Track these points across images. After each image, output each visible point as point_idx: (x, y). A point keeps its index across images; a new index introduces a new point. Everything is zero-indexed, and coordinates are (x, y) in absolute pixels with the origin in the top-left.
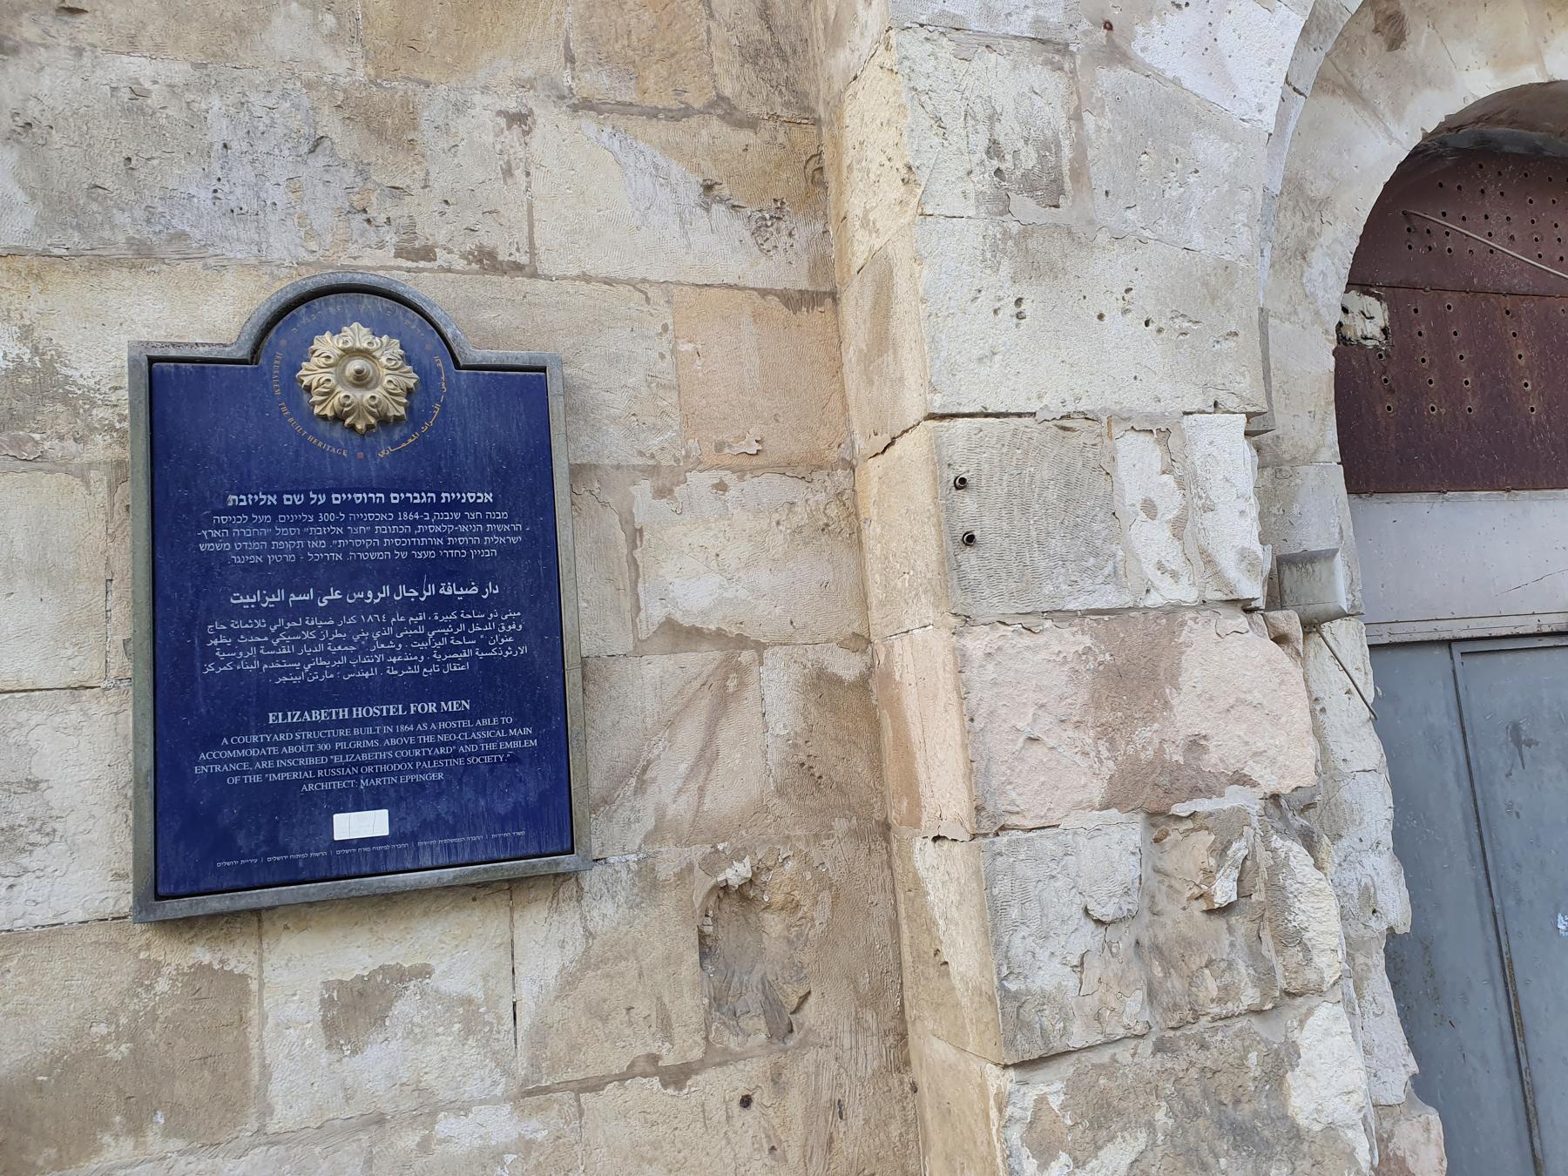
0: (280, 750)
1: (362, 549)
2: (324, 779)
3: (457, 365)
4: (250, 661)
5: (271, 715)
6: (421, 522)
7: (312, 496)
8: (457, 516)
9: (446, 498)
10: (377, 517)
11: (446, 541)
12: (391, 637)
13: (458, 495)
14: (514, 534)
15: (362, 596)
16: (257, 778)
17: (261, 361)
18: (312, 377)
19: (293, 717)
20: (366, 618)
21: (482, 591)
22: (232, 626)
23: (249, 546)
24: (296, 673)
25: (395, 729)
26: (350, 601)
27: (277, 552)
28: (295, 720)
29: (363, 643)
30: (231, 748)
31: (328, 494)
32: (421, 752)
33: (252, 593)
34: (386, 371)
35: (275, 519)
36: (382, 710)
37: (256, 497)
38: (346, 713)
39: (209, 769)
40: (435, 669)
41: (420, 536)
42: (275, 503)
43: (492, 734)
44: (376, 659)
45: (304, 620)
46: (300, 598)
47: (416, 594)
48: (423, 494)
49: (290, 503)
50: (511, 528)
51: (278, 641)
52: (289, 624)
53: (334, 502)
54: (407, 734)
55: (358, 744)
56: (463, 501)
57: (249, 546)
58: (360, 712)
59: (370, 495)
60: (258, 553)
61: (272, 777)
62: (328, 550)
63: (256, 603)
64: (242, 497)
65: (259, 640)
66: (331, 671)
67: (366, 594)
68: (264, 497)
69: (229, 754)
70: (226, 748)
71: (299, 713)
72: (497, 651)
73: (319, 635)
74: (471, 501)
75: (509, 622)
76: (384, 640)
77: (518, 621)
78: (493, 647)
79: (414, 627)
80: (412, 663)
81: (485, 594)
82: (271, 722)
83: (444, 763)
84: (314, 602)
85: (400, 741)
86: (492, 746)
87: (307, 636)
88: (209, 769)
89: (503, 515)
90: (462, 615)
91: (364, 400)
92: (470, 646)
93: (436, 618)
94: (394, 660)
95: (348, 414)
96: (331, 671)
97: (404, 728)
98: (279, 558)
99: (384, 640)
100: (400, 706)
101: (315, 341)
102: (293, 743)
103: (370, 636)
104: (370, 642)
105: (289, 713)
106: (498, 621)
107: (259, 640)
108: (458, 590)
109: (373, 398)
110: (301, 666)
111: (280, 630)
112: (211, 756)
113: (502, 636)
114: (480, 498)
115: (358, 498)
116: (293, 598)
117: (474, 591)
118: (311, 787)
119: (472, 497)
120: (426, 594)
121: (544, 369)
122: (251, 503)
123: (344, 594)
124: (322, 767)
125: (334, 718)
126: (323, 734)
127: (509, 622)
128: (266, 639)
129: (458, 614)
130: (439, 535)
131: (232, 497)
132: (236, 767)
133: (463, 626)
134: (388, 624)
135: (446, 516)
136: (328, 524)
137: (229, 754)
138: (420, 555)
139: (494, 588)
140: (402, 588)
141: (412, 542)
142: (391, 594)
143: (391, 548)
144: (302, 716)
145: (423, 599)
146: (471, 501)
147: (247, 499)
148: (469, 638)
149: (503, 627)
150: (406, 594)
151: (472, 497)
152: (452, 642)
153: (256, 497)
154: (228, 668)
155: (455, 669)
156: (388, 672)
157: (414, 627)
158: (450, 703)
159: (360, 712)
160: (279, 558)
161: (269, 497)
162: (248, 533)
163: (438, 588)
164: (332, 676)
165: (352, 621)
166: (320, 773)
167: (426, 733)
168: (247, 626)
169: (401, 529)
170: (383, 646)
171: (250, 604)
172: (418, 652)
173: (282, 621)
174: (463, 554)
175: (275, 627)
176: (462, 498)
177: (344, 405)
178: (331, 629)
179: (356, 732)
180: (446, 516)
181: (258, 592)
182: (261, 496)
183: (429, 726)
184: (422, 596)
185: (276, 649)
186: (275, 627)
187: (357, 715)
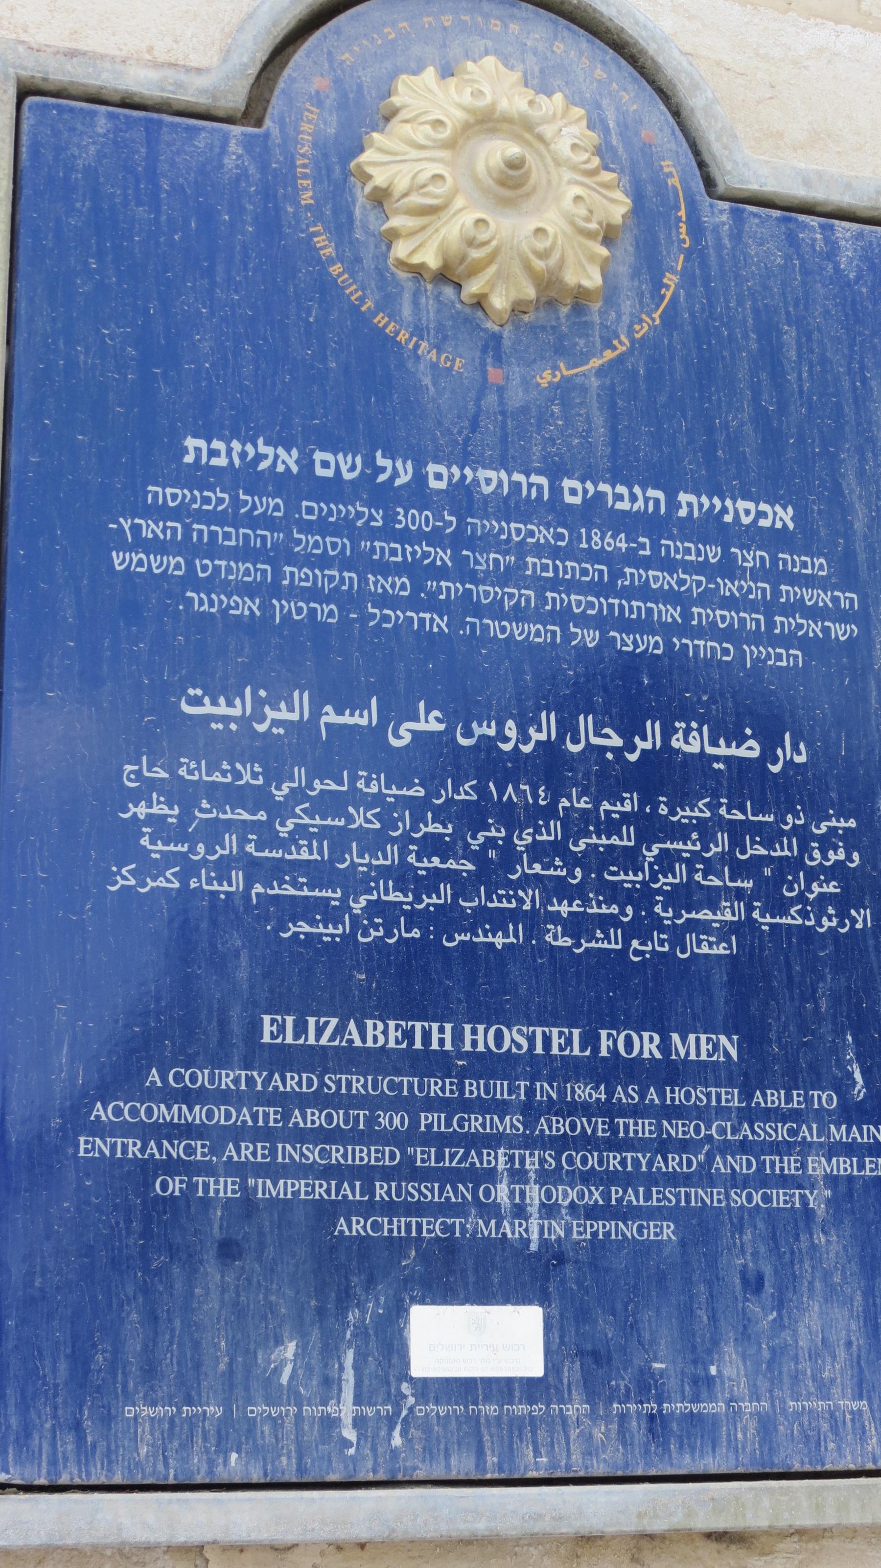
0: (286, 1116)
1: (496, 611)
2: (390, 1209)
3: (709, 183)
4: (223, 869)
5: (267, 1019)
6: (632, 558)
7: (381, 461)
8: (713, 554)
9: (690, 505)
10: (531, 534)
11: (687, 615)
12: (559, 848)
13: (716, 501)
14: (843, 617)
15: (492, 732)
17: (268, 123)
18: (394, 168)
19: (320, 1031)
20: (501, 791)
21: (768, 755)
22: (182, 772)
23: (229, 570)
24: (332, 916)
25: (562, 1092)
26: (464, 742)
27: (293, 593)
28: (324, 1041)
29: (492, 854)
30: (169, 1096)
31: (556, 473)
32: (623, 1162)
33: (232, 693)
34: (567, 175)
35: (292, 506)
36: (531, 1039)
37: (249, 448)
38: (448, 1036)
39: (113, 1147)
40: (658, 944)
41: (628, 593)
42: (295, 469)
43: (791, 1132)
44: (521, 901)
45: (354, 779)
46: (346, 719)
47: (617, 741)
48: (637, 490)
49: (329, 473)
50: (835, 600)
51: (290, 824)
52: (317, 784)
53: (433, 484)
54: (587, 1109)
55: (475, 1124)
57: (229, 570)
58: (480, 1037)
60: (249, 590)
62: (413, 602)
63: (241, 720)
64: (217, 444)
65: (246, 816)
66: (412, 920)
67: (501, 726)
68: (269, 450)
69: (162, 1113)
70: (151, 1095)
71: (334, 1022)
72: (804, 914)
73: (389, 823)
74: (746, 520)
75: (827, 843)
76: (537, 852)
77: (850, 840)
78: (792, 901)
79: (611, 827)
80: (606, 922)
81: (775, 762)
82: (266, 1039)
85: (573, 1127)
87: (359, 821)
88: (113, 1147)
89: (819, 567)
90: (723, 811)
92: (739, 894)
93: (663, 810)
94: (564, 909)
95: (475, 270)
96: (412, 920)
97: (583, 1092)
98: (299, 611)
99: (537, 852)
100: (576, 1032)
101: (400, 87)
102: (320, 1100)
103: (508, 839)
104: (509, 856)
105: (312, 1021)
106: (803, 835)
107: (246, 816)
108: (714, 743)
109: (540, 232)
110: (344, 900)
111: (298, 795)
112: (118, 1112)
113: (812, 875)
114: (764, 515)
115: (488, 481)
116: (330, 716)
117: (750, 750)
118: (358, 1226)
119: (747, 512)
120: (641, 745)
122: (237, 462)
123: (449, 718)
124: (387, 1174)
125: (418, 1045)
126: (392, 1086)
127: (827, 843)
128: (262, 816)
129: (713, 807)
130: (670, 597)
131: (191, 443)
132: (177, 1150)
133: (723, 839)
134: (550, 812)
135: (688, 551)
136: (419, 537)
137: (162, 1113)
138: (626, 643)
139: (796, 749)
140: (585, 723)
141: (611, 606)
142: (561, 737)
143: (563, 617)
144: (340, 1030)
145: (633, 757)
146: (746, 520)
147: (229, 451)
148: (739, 870)
149: (817, 854)
150: (595, 741)
151: (747, 512)
152: (698, 877)
153: (249, 448)
154: (169, 881)
155: (705, 950)
156: (549, 938)
157: (611, 827)
158: (692, 1037)
159: (480, 1037)
160: (299, 611)
161: (281, 451)
162: (227, 536)
163: (668, 732)
164: (416, 933)
165: (467, 793)
166: (380, 1191)
167: (636, 1112)
168: (217, 777)
169: (585, 572)
170: (537, 868)
172: (613, 894)
173: (300, 773)
174: (726, 652)
175: (286, 788)
176: (724, 510)
177: (471, 243)
178: (419, 809)
179: (473, 1089)
180: (688, 551)
181: (248, 691)
182: (263, 449)
183: (643, 1095)
184: (632, 748)
185: (284, 844)
186: (286, 788)
187: (474, 1043)
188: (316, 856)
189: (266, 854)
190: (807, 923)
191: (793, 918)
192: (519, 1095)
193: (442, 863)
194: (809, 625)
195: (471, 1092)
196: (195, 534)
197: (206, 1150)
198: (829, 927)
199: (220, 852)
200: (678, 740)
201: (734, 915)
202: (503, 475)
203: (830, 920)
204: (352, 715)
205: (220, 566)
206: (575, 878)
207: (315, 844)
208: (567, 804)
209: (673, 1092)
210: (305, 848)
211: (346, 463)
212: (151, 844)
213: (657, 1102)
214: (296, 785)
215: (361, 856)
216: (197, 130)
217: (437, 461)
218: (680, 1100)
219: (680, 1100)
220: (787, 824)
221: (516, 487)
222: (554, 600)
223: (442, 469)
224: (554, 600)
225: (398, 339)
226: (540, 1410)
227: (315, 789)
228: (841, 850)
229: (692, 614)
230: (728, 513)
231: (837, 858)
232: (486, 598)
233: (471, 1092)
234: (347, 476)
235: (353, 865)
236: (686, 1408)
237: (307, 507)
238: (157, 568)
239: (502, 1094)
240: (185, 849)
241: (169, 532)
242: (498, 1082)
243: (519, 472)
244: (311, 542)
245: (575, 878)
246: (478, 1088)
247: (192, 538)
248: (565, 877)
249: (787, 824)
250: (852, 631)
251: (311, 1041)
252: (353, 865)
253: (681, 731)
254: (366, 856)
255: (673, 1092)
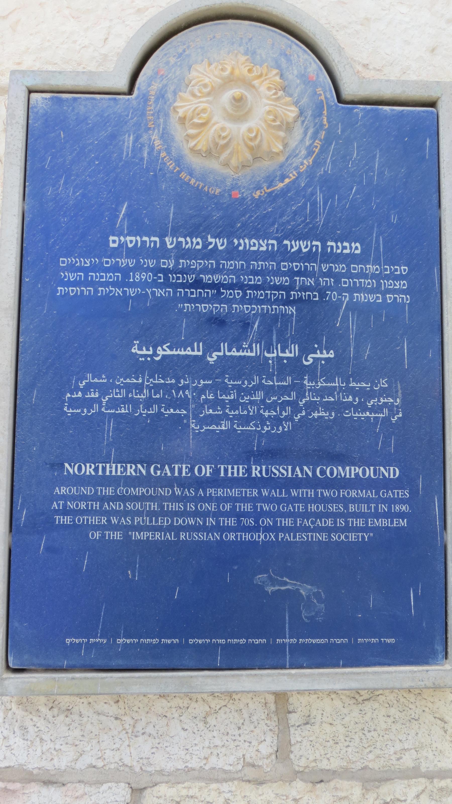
3: (340, 99)
16: (117, 536)
56: (241, 248)
59: (145, 238)
61: (136, 536)
64: (346, 244)
83: (308, 536)
84: (297, 360)
86: (360, 523)
91: (241, 132)
109: (250, 130)
121: (433, 104)
160: (205, 308)
171: (146, 356)
188: (127, 411)
189: (109, 411)
190: (258, 429)
191: (252, 427)
192: (371, 510)
193: (174, 411)
194: (116, 290)
195: (352, 509)
196: (90, 277)
197: (327, 537)
198: (267, 430)
199: (92, 411)
200: (135, 349)
201: (225, 427)
202: (138, 238)
203: (268, 427)
204: (176, 350)
205: (268, 293)
206: (332, 416)
207: (127, 406)
208: (204, 397)
209: (311, 506)
210: (123, 408)
211: (220, 242)
212: (68, 410)
213: (57, 508)
214: (88, 381)
215: (355, 413)
216: (353, 109)
217: (113, 235)
218: (314, 510)
219: (314, 510)
220: (181, 383)
221: (143, 243)
222: (294, 295)
223: (116, 238)
224: (61, 290)
225: (190, 183)
226: (157, 641)
227: (381, 402)
228: (97, 393)
229: (99, 290)
230: (241, 246)
231: (384, 401)
232: (238, 296)
233: (352, 509)
234: (220, 248)
235: (141, 414)
236: (310, 641)
237: (106, 261)
238: (372, 300)
239: (364, 510)
240: (80, 411)
241: (167, 293)
242: (363, 505)
243: (181, 237)
244: (284, 280)
245: (332, 416)
246: (355, 508)
247: (88, 279)
248: (80, 413)
249: (181, 383)
250: (138, 291)
251: (300, 490)
252: (141, 414)
253: (136, 345)
254: (146, 410)
255: (311, 506)
